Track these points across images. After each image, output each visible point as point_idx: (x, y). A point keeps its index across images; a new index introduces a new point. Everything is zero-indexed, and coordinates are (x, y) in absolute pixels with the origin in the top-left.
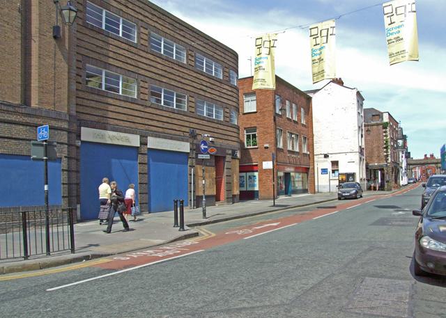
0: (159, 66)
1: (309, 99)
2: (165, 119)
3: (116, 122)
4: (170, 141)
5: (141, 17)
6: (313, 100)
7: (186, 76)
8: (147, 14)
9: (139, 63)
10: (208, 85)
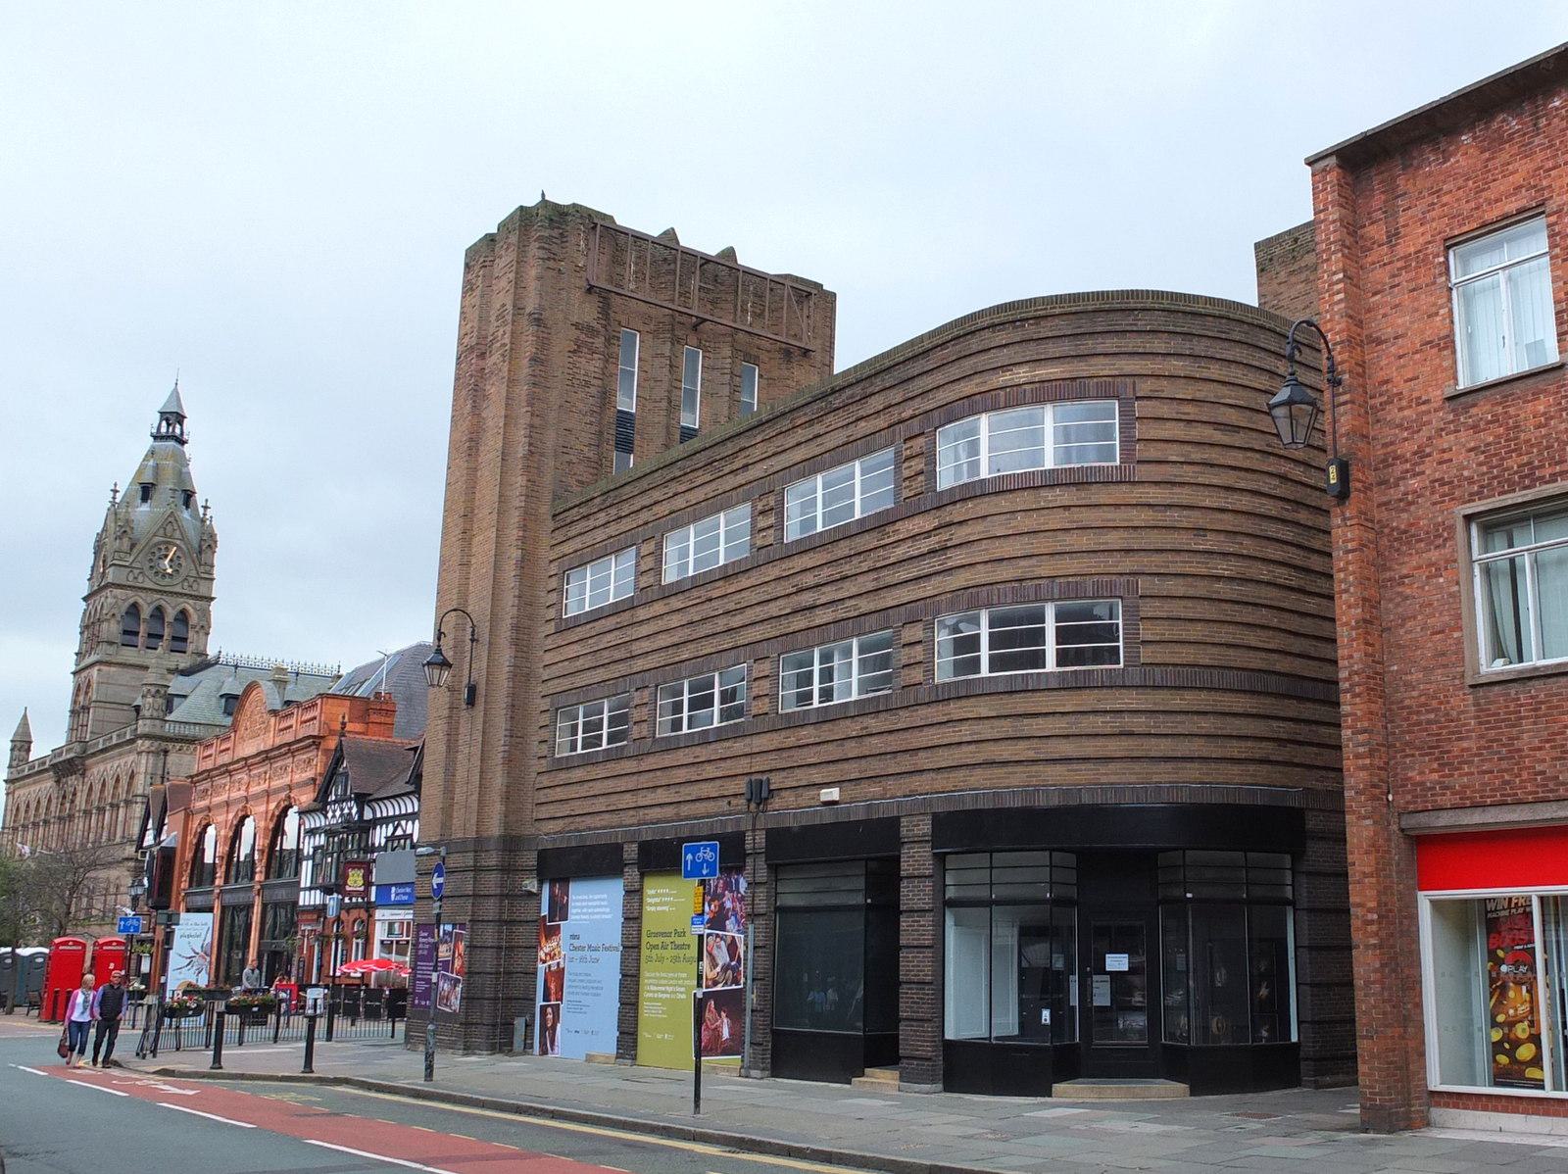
5: (645, 516)
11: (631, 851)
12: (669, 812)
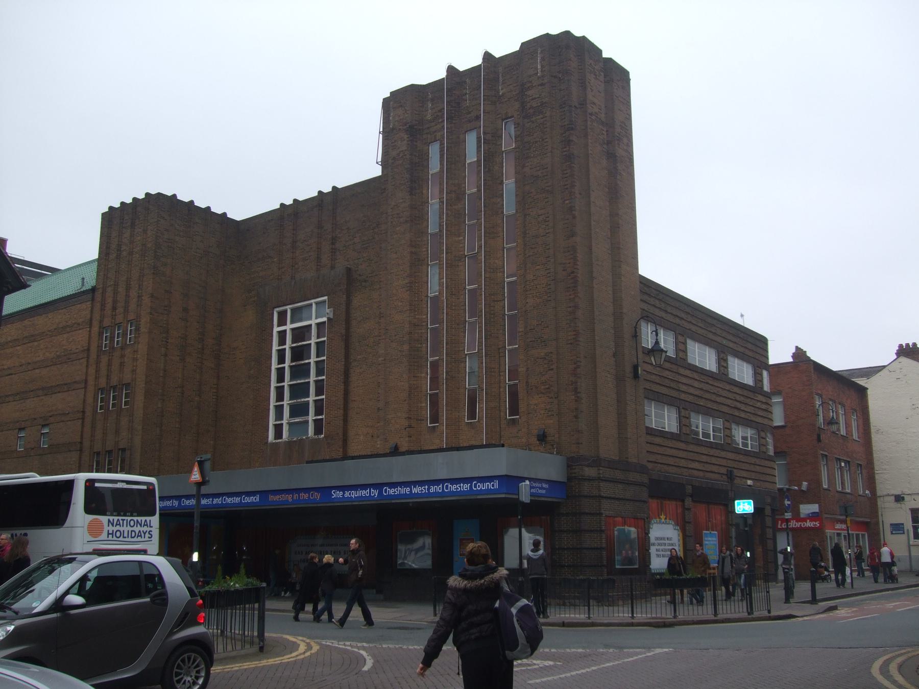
0: (696, 384)
1: (862, 392)
2: (704, 458)
3: (666, 467)
4: (43, 301)
5: (678, 321)
6: (869, 392)
7: (722, 392)
8: (683, 315)
9: (681, 385)
10: (742, 399)
11: (689, 489)
12: (701, 474)
